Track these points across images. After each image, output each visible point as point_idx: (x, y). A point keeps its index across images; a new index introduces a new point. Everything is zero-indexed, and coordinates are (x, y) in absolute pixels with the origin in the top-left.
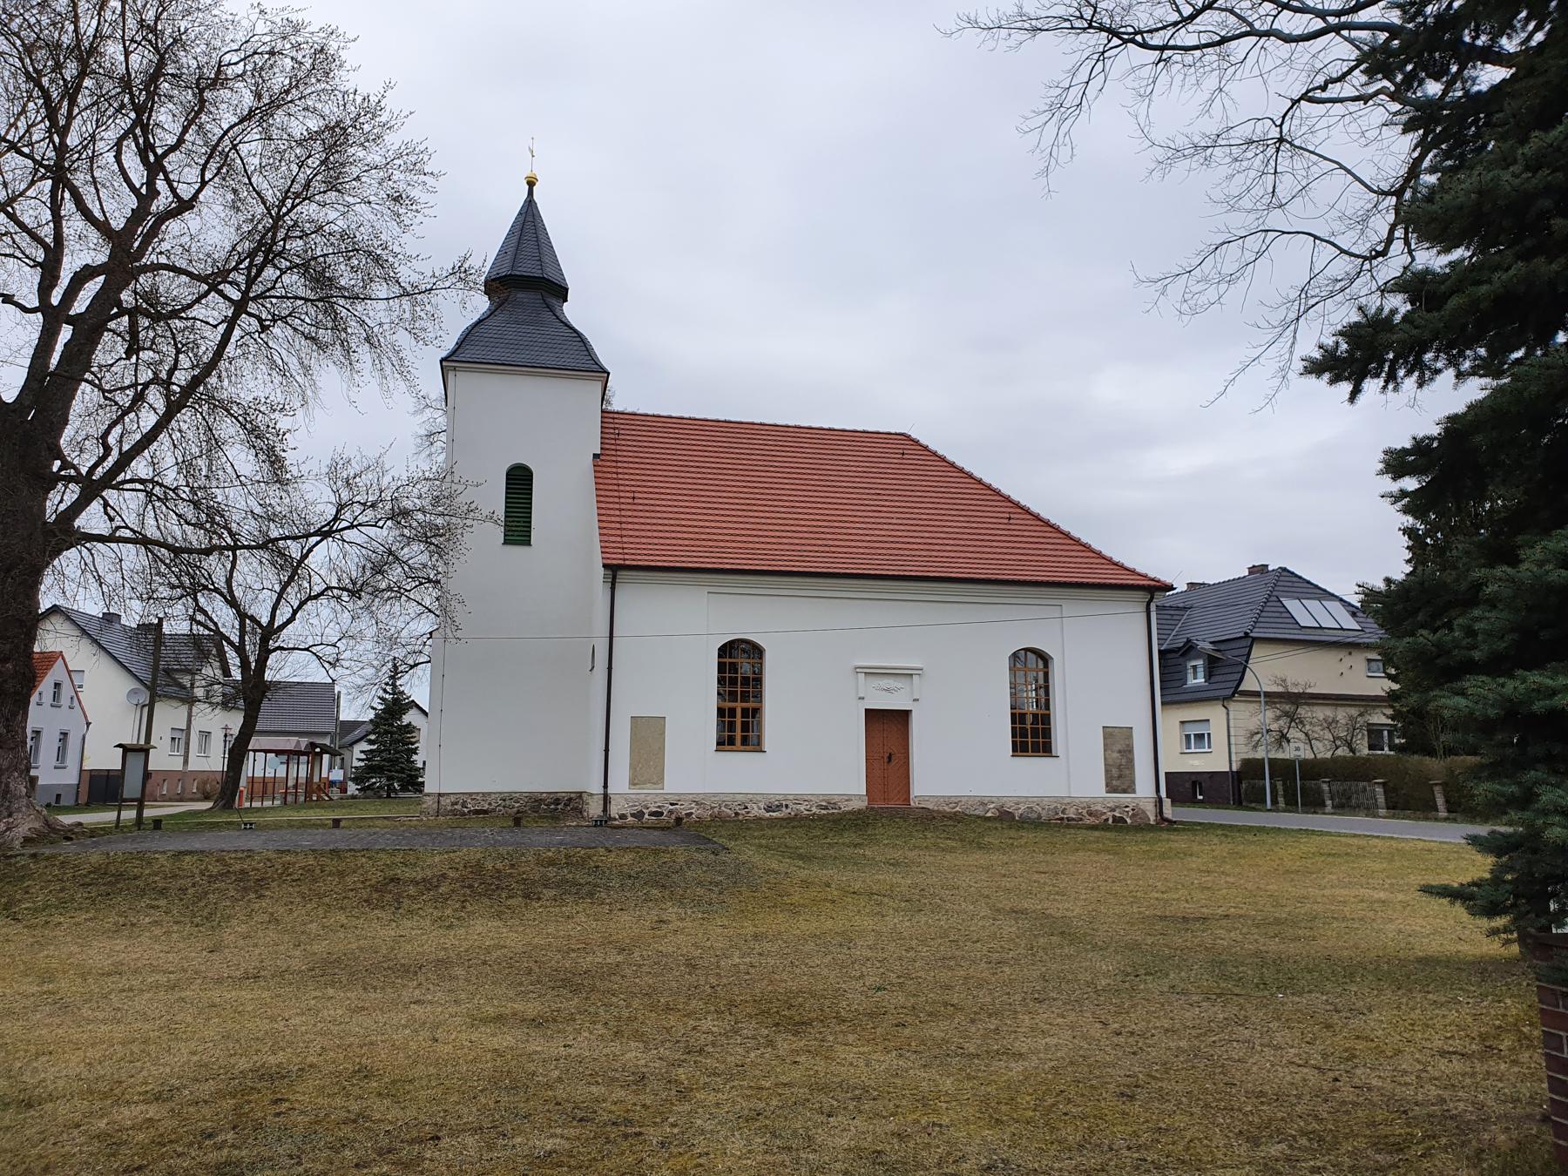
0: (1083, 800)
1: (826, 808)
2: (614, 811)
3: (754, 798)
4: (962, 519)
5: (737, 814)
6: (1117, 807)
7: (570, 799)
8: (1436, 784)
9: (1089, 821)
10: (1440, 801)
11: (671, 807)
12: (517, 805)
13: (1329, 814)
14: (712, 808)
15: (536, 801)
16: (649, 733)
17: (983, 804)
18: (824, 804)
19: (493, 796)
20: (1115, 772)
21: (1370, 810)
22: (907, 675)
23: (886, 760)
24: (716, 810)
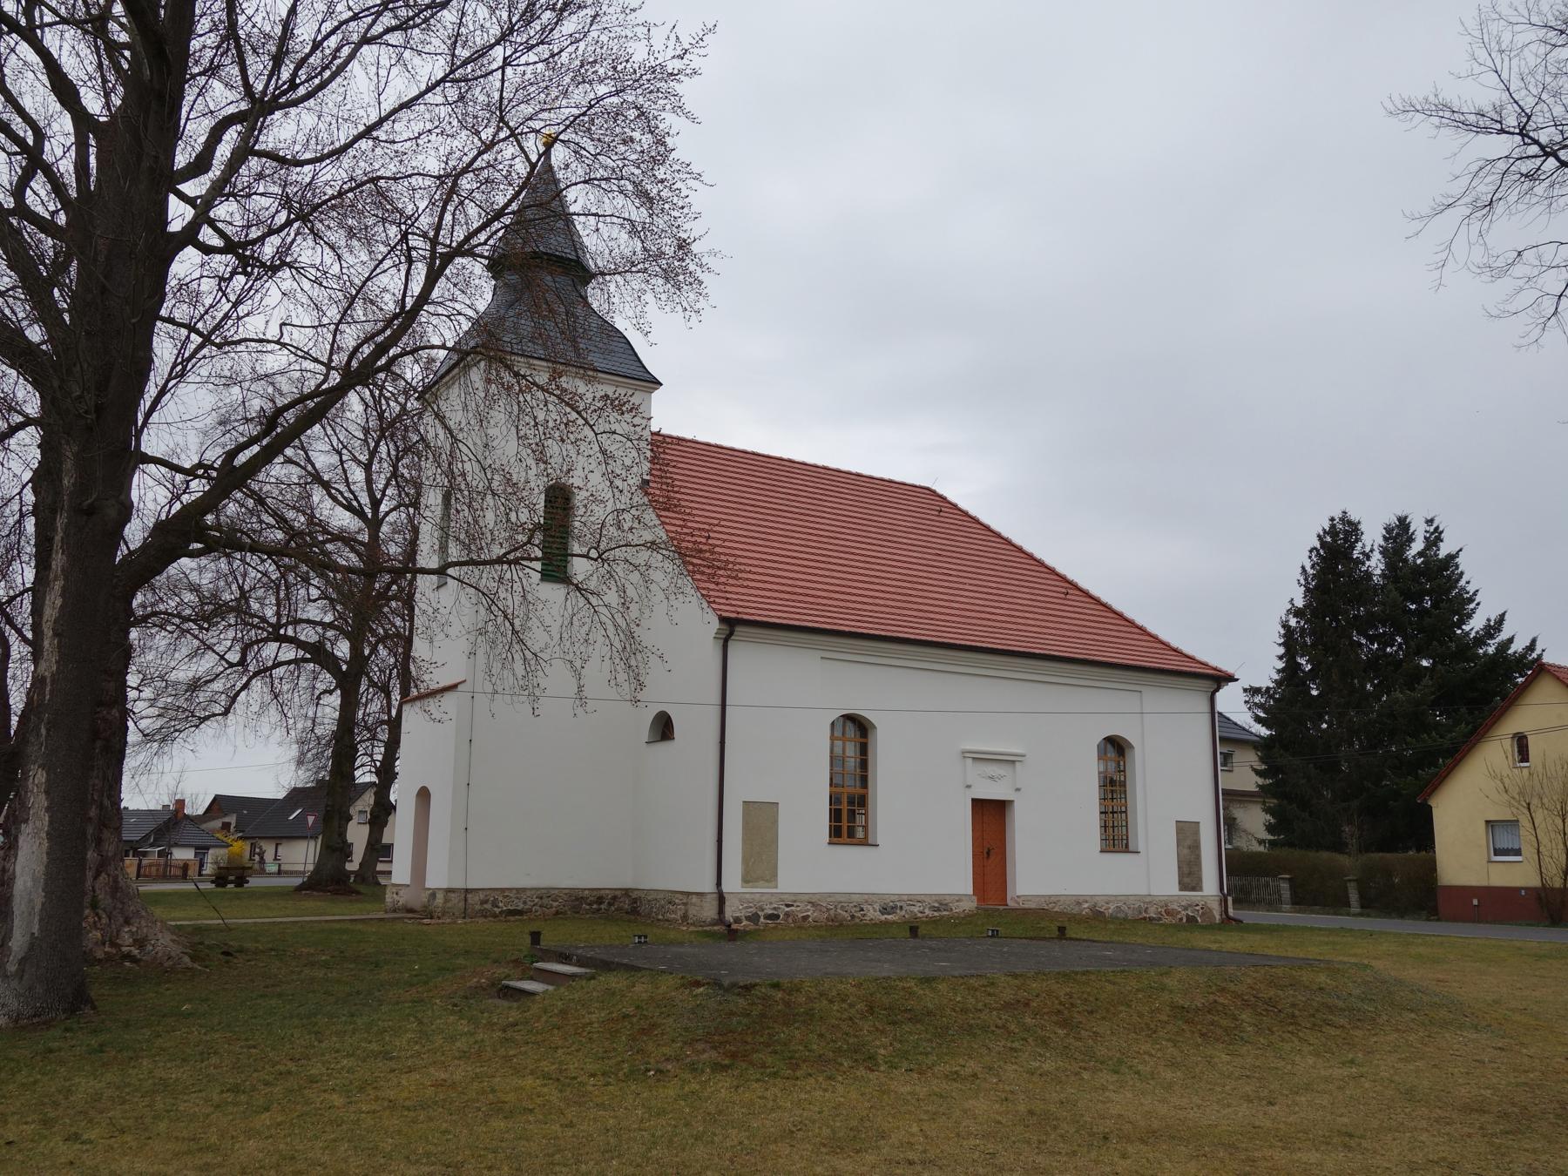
0: (1161, 898)
1: (938, 910)
2: (729, 914)
3: (869, 898)
4: (1025, 590)
5: (853, 917)
6: (1190, 905)
7: (615, 898)
8: (1350, 881)
9: (1167, 920)
10: (1354, 897)
11: (787, 909)
12: (555, 904)
13: (1354, 915)
14: (828, 910)
15: (577, 899)
16: (762, 819)
17: (1079, 904)
18: (936, 905)
19: (528, 893)
20: (1186, 870)
21: (1273, 904)
22: (1010, 761)
23: (985, 855)
24: (832, 912)
